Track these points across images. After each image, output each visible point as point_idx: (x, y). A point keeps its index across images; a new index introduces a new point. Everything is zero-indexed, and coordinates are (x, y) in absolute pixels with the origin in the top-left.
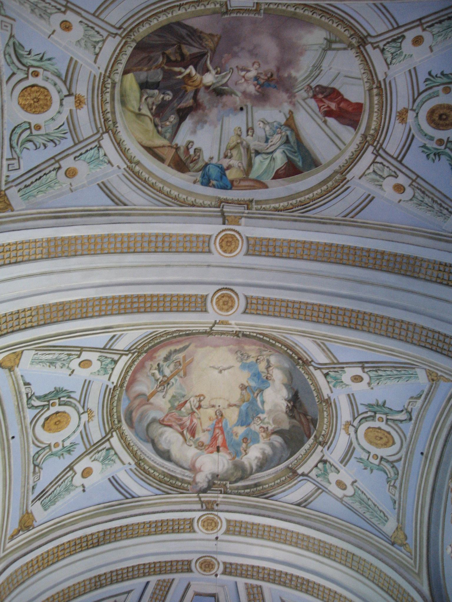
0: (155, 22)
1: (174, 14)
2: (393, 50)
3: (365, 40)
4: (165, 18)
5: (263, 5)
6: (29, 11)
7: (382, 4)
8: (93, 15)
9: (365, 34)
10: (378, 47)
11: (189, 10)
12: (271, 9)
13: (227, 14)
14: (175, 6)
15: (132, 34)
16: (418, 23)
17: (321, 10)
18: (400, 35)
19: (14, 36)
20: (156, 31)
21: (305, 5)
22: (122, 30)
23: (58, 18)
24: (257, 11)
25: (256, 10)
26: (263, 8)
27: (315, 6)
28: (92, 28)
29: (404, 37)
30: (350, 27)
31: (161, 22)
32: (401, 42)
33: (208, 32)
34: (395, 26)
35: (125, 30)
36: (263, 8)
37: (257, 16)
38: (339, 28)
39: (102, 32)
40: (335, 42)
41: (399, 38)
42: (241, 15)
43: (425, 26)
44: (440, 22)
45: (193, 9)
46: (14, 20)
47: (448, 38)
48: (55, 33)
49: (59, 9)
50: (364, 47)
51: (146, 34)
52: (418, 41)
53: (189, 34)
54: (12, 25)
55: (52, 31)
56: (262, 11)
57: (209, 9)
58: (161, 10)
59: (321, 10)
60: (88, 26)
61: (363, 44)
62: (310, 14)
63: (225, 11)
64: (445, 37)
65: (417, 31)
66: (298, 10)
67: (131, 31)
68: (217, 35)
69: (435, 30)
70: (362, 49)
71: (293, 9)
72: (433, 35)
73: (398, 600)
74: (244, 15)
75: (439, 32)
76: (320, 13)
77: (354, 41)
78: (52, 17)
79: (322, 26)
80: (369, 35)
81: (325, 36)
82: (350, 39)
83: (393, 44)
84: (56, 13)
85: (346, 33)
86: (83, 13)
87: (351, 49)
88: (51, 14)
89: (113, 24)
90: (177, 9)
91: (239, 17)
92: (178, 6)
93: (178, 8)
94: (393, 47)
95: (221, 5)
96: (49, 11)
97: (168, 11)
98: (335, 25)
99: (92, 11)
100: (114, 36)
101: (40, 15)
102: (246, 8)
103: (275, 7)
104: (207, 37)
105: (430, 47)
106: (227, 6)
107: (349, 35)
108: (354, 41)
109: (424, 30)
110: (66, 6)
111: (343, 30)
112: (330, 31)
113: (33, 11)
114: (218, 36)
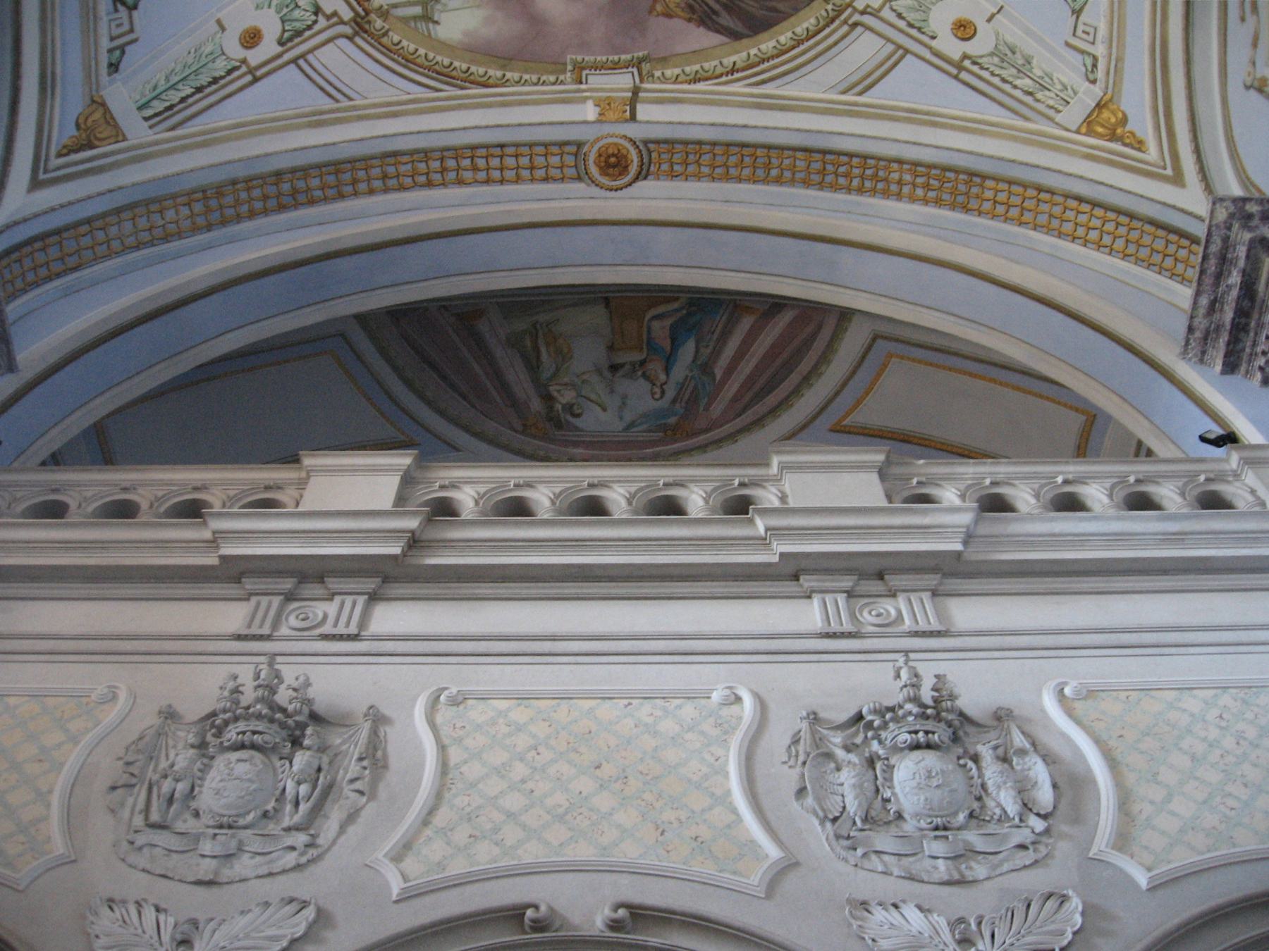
0: (782, 39)
1: (744, 54)
2: (297, 13)
3: (357, 29)
4: (763, 47)
5: (569, 80)
6: (1034, 62)
7: (337, 101)
8: (907, 51)
9: (358, 40)
10: (328, 18)
11: (716, 62)
12: (551, 73)
13: (638, 58)
14: (743, 70)
15: (832, 14)
16: (258, 73)
17: (453, 78)
18: (289, 45)
19: (1073, 12)
20: (784, 19)
21: (485, 85)
22: (850, 22)
24: (579, 68)
25: (583, 68)
26: (569, 74)
27: (467, 84)
28: (911, 25)
29: (281, 43)
30: (389, 51)
31: (771, 39)
32: (284, 31)
33: (677, 23)
34: (301, 62)
35: (845, 22)
36: (569, 74)
37: (579, 58)
38: (412, 47)
39: (891, 17)
40: (415, 18)
41: (290, 39)
42: (611, 58)
43: (244, 69)
44: (215, 80)
45: (706, 66)
46: (1067, 44)
47: (193, 50)
48: (989, 15)
49: (974, 63)
50: (357, 14)
51: (802, 13)
52: (252, 38)
53: (714, 17)
54: (1074, 35)
55: (994, 19)
56: (569, 67)
57: (676, 66)
58: (772, 62)
59: (453, 78)
60: (919, 29)
61: (359, 20)
62: (473, 69)
63: (643, 65)
64: (198, 54)
65: (256, 56)
66: (499, 74)
67: (833, 21)
68: (658, 15)
69: (220, 66)
70: (360, 10)
71: (509, 75)
72: (223, 54)
73: (5, 262)
74: (604, 59)
75: (214, 61)
76: (454, 73)
77: (379, 23)
78: (990, 48)
79: (445, 47)
80: (350, 38)
81: (438, 27)
82: (387, 27)
83: (298, 25)
84: (981, 57)
85: (396, 38)
86: (928, 55)
87: (381, 7)
88: (992, 54)
89: (867, 32)
90: (740, 65)
91: (617, 54)
92: (738, 71)
93: (736, 67)
94: (296, 20)
95: (653, 76)
96: (996, 60)
97: (757, 60)
98: (422, 51)
99: (909, 56)
100: (869, 10)
101: (1014, 53)
102: (603, 72)
103: (544, 78)
104: (679, 11)
105: (223, 29)
106: (640, 74)
107: (391, 34)
108: (379, 23)
109: (244, 61)
110: (960, 68)
111: (405, 43)
112: (429, 39)
113: (1028, 61)
114: (655, 13)
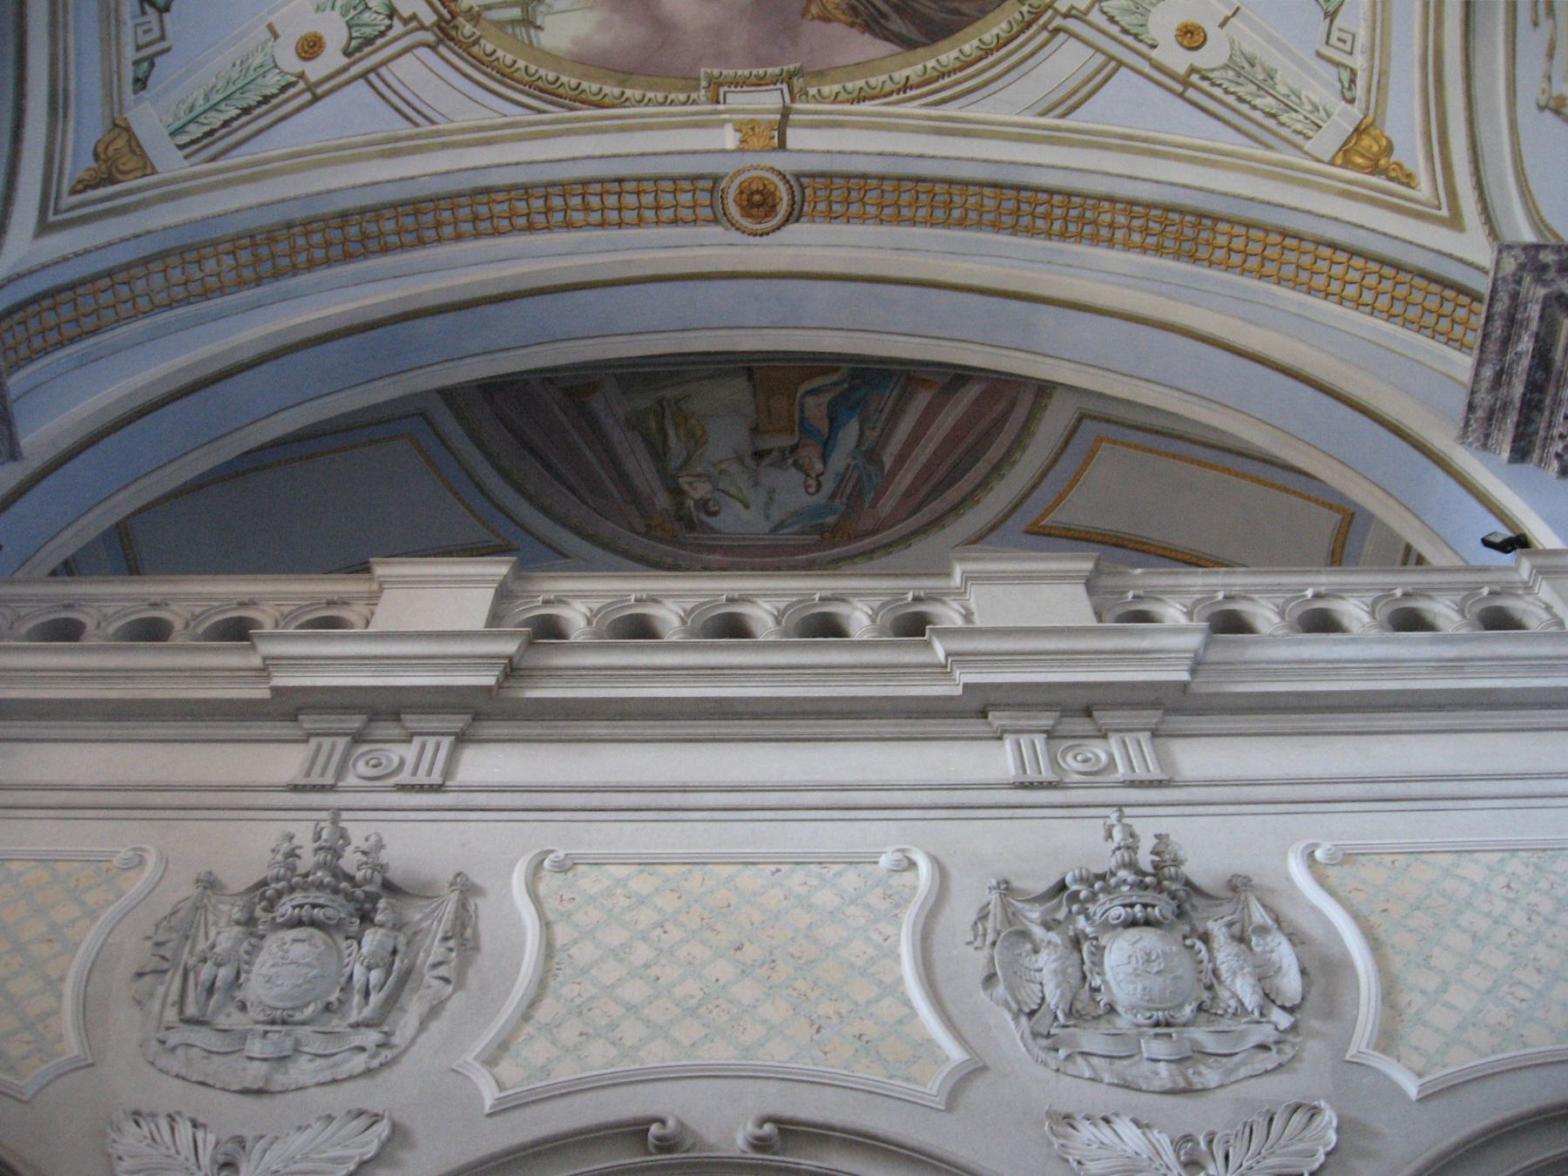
0: (967, 48)
1: (919, 67)
2: (367, 17)
4: (943, 58)
5: (703, 99)
6: (1278, 77)
7: (417, 125)
8: (1120, 63)
9: (442, 49)
10: (406, 22)
11: (885, 77)
12: (681, 90)
13: (788, 72)
14: (918, 86)
15: (1027, 17)
16: (319, 91)
17: (560, 96)
18: (358, 55)
19: (1326, 15)
20: (969, 24)
21: (599, 106)
22: (1050, 27)
23: (1210, 57)
24: (715, 84)
25: (721, 85)
26: (703, 92)
27: (577, 104)
28: (1125, 31)
29: (347, 53)
30: (481, 63)
31: (953, 48)
32: (351, 38)
33: (837, 29)
34: (372, 77)
35: (1044, 27)
36: (703, 92)
37: (716, 72)
38: (509, 59)
39: (1101, 21)
40: (513, 22)
41: (359, 49)
42: (754, 72)
43: (301, 85)
44: (266, 99)
45: (873, 81)
46: (1319, 55)
47: (238, 62)
48: (1222, 18)
49: (1204, 78)
50: (441, 17)
51: (990, 16)
52: (311, 47)
53: (882, 21)
54: (1327, 43)
55: (1229, 24)
56: (704, 83)
57: (835, 82)
58: (953, 77)
59: (560, 96)
60: (1136, 36)
61: (443, 24)
62: (585, 85)
63: (795, 80)
64: (245, 67)
65: (316, 70)
66: (617, 91)
67: (1029, 25)
68: (813, 19)
69: (272, 82)
70: (445, 12)
71: (629, 93)
72: (276, 66)
74: (747, 72)
75: (264, 75)
76: (561, 91)
77: (468, 29)
78: (1223, 59)
79: (550, 58)
80: (433, 48)
81: (541, 34)
82: (478, 33)
83: (368, 31)
84: (1213, 70)
85: (489, 48)
86: (1147, 69)
87: (471, 8)
88: (1226, 67)
89: (1072, 40)
90: (914, 80)
91: (762, 66)
92: (911, 88)
93: (910, 83)
94: (366, 25)
95: (806, 94)
96: (1231, 74)
97: (936, 74)
98: (521, 64)
99: (1123, 70)
100: (1074, 12)
101: (1253, 65)
102: (745, 89)
103: (672, 96)
104: (839, 14)
105: (276, 36)
106: (791, 92)
107: (483, 41)
108: (468, 29)
109: (301, 76)
111: (500, 53)
112: (531, 49)
113: (1270, 76)
114: (809, 16)
